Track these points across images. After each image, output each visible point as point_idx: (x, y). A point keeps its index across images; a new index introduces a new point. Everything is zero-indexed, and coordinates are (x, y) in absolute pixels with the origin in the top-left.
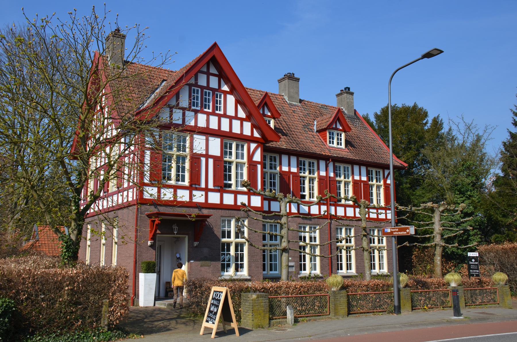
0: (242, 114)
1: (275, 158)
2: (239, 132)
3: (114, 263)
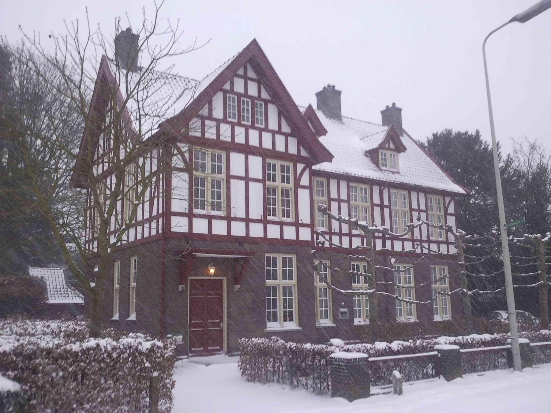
0: (286, 128)
1: (220, 157)
2: (284, 150)
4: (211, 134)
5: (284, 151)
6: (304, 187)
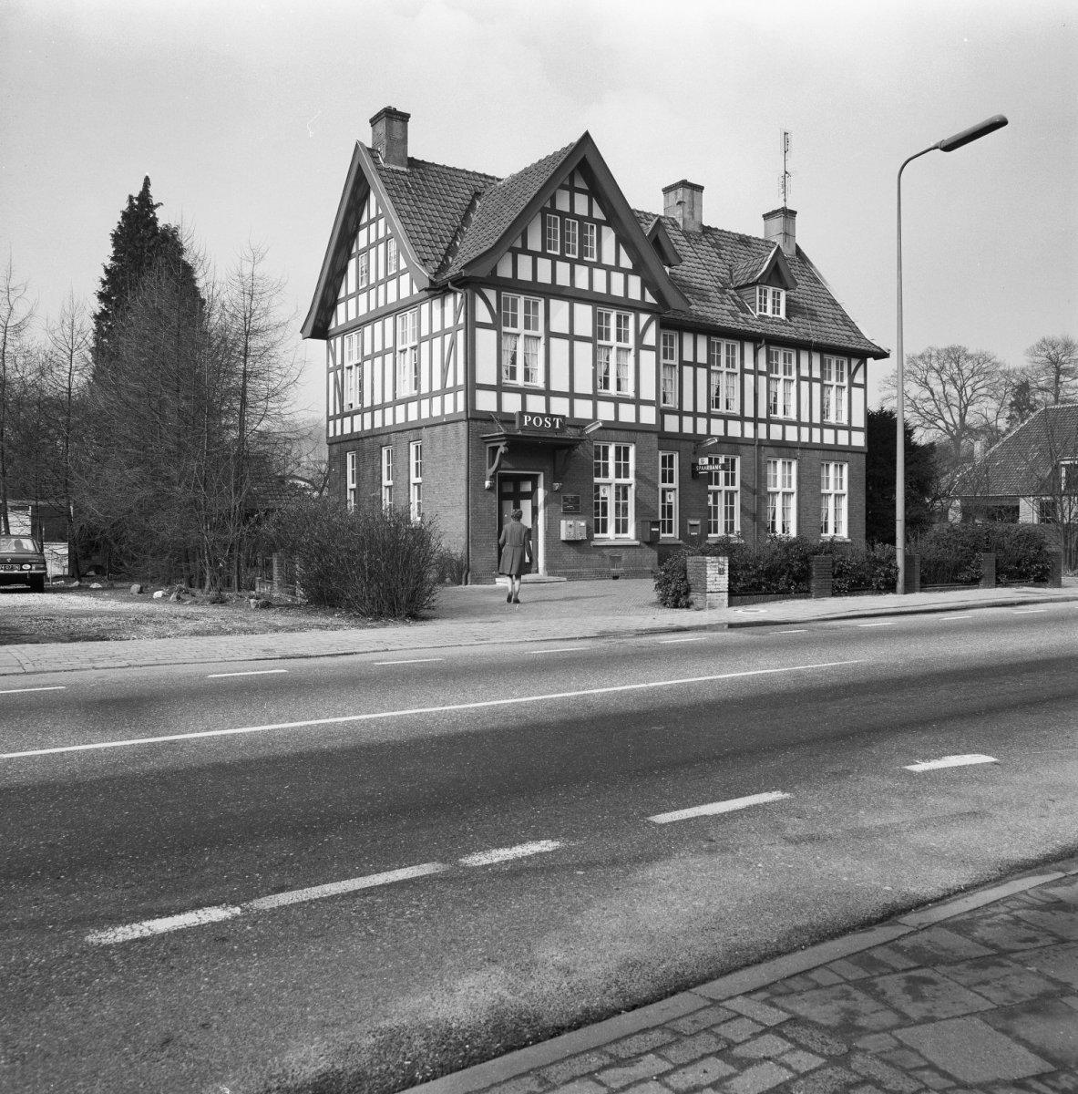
0: (626, 262)
3: (793, 533)
4: (525, 274)
5: (587, 289)
6: (649, 348)
